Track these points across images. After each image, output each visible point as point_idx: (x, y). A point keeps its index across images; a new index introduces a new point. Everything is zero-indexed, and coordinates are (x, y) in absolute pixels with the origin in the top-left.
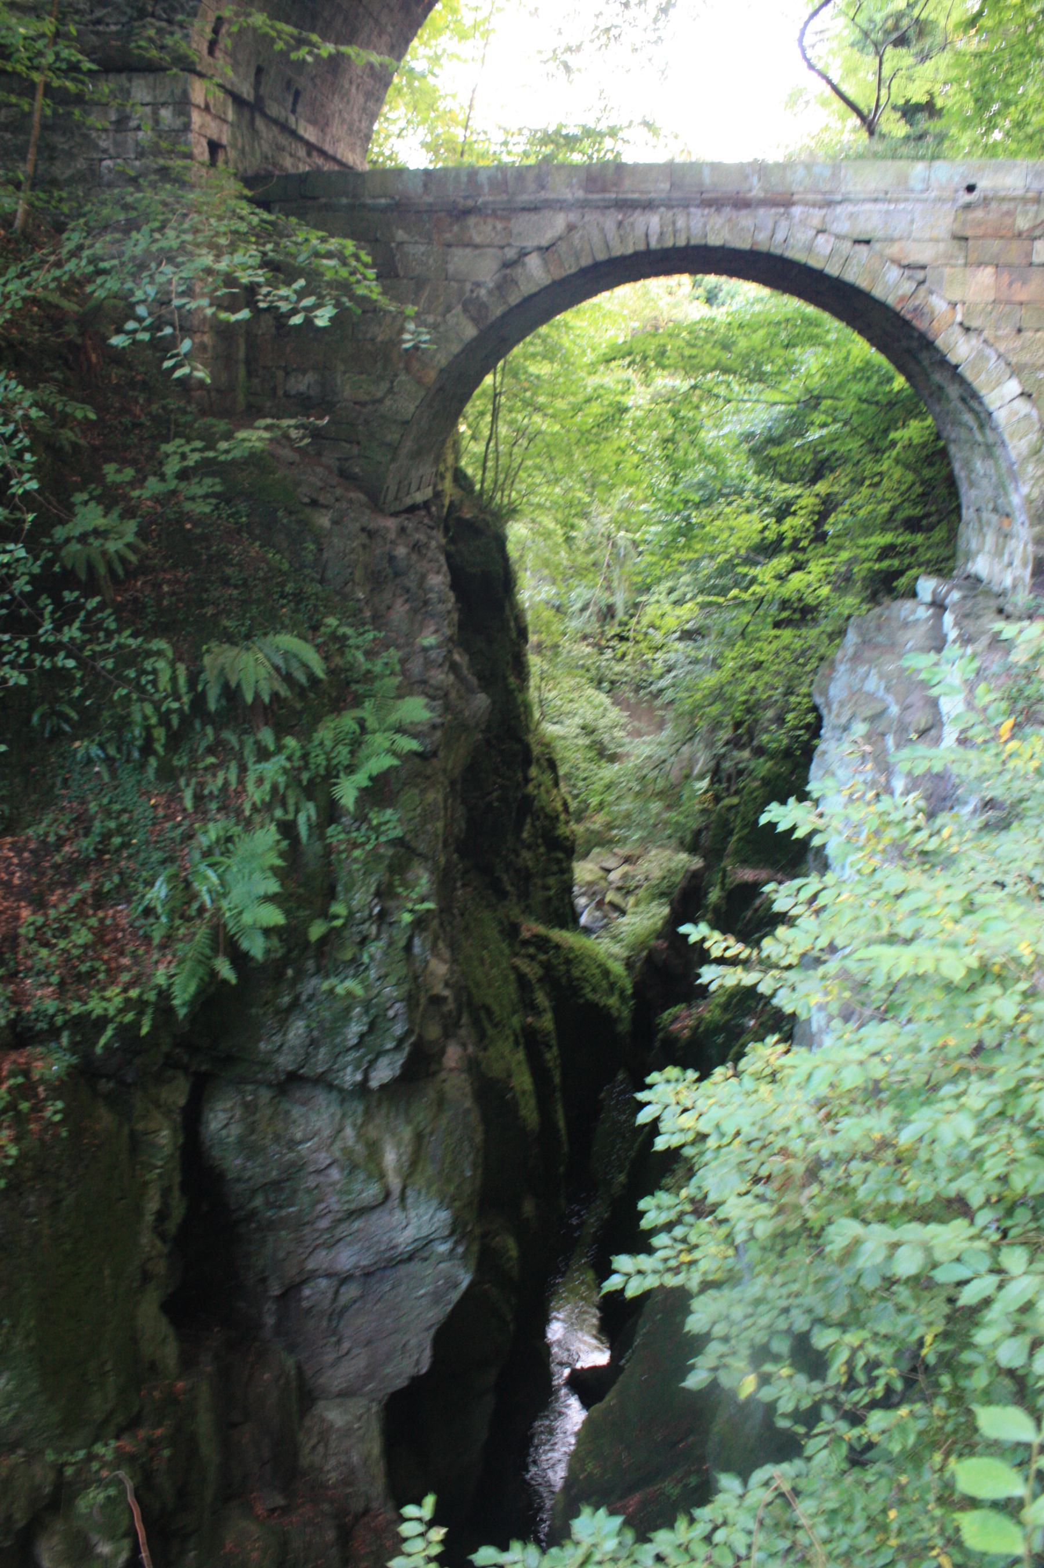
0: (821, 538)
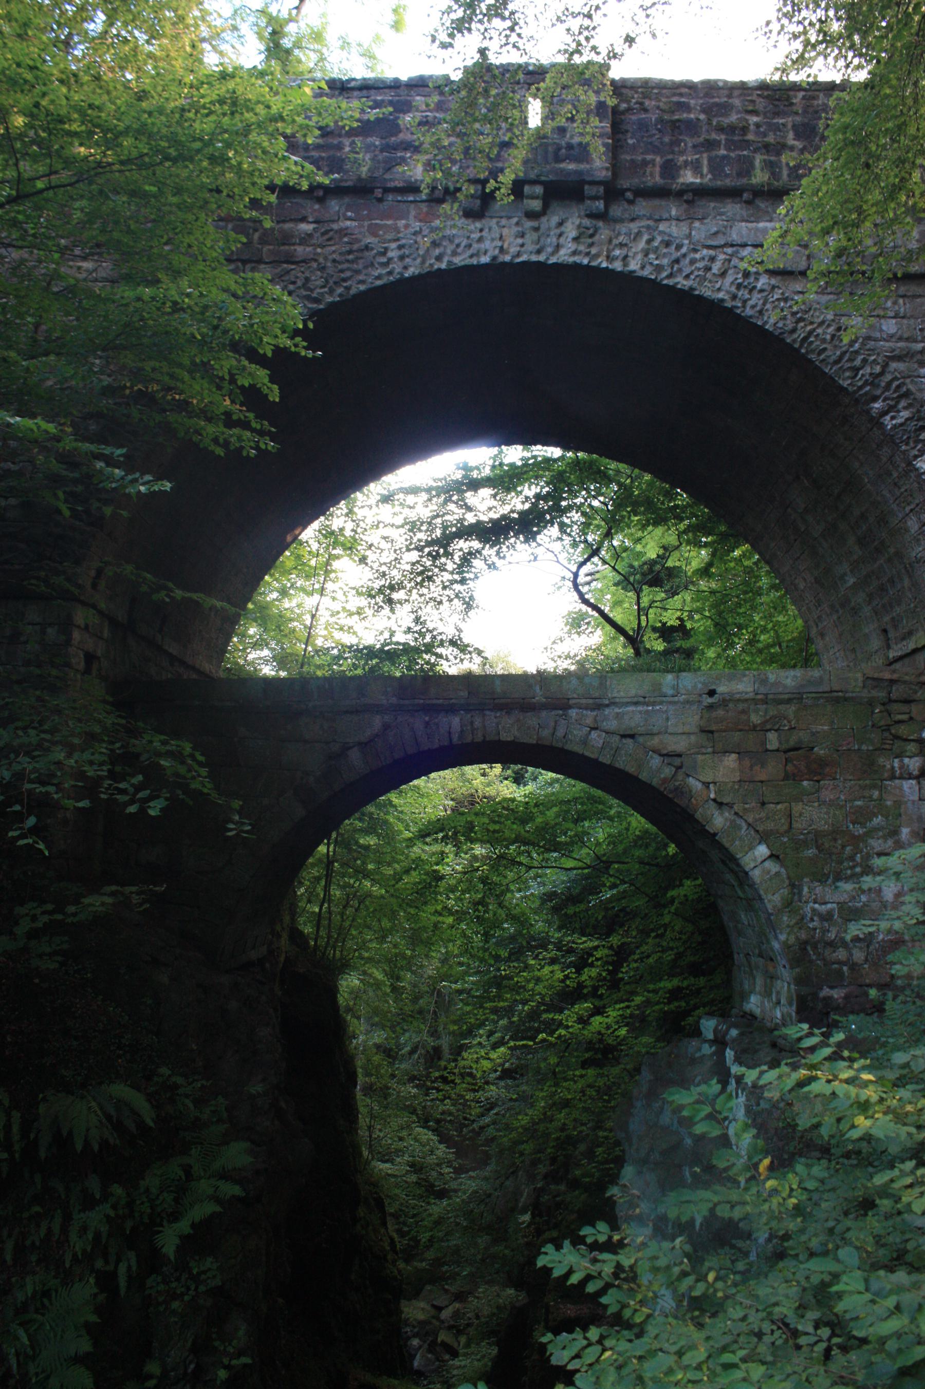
0: (615, 984)
